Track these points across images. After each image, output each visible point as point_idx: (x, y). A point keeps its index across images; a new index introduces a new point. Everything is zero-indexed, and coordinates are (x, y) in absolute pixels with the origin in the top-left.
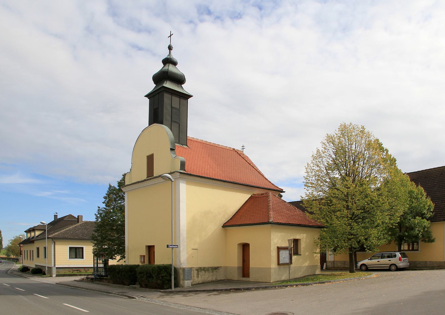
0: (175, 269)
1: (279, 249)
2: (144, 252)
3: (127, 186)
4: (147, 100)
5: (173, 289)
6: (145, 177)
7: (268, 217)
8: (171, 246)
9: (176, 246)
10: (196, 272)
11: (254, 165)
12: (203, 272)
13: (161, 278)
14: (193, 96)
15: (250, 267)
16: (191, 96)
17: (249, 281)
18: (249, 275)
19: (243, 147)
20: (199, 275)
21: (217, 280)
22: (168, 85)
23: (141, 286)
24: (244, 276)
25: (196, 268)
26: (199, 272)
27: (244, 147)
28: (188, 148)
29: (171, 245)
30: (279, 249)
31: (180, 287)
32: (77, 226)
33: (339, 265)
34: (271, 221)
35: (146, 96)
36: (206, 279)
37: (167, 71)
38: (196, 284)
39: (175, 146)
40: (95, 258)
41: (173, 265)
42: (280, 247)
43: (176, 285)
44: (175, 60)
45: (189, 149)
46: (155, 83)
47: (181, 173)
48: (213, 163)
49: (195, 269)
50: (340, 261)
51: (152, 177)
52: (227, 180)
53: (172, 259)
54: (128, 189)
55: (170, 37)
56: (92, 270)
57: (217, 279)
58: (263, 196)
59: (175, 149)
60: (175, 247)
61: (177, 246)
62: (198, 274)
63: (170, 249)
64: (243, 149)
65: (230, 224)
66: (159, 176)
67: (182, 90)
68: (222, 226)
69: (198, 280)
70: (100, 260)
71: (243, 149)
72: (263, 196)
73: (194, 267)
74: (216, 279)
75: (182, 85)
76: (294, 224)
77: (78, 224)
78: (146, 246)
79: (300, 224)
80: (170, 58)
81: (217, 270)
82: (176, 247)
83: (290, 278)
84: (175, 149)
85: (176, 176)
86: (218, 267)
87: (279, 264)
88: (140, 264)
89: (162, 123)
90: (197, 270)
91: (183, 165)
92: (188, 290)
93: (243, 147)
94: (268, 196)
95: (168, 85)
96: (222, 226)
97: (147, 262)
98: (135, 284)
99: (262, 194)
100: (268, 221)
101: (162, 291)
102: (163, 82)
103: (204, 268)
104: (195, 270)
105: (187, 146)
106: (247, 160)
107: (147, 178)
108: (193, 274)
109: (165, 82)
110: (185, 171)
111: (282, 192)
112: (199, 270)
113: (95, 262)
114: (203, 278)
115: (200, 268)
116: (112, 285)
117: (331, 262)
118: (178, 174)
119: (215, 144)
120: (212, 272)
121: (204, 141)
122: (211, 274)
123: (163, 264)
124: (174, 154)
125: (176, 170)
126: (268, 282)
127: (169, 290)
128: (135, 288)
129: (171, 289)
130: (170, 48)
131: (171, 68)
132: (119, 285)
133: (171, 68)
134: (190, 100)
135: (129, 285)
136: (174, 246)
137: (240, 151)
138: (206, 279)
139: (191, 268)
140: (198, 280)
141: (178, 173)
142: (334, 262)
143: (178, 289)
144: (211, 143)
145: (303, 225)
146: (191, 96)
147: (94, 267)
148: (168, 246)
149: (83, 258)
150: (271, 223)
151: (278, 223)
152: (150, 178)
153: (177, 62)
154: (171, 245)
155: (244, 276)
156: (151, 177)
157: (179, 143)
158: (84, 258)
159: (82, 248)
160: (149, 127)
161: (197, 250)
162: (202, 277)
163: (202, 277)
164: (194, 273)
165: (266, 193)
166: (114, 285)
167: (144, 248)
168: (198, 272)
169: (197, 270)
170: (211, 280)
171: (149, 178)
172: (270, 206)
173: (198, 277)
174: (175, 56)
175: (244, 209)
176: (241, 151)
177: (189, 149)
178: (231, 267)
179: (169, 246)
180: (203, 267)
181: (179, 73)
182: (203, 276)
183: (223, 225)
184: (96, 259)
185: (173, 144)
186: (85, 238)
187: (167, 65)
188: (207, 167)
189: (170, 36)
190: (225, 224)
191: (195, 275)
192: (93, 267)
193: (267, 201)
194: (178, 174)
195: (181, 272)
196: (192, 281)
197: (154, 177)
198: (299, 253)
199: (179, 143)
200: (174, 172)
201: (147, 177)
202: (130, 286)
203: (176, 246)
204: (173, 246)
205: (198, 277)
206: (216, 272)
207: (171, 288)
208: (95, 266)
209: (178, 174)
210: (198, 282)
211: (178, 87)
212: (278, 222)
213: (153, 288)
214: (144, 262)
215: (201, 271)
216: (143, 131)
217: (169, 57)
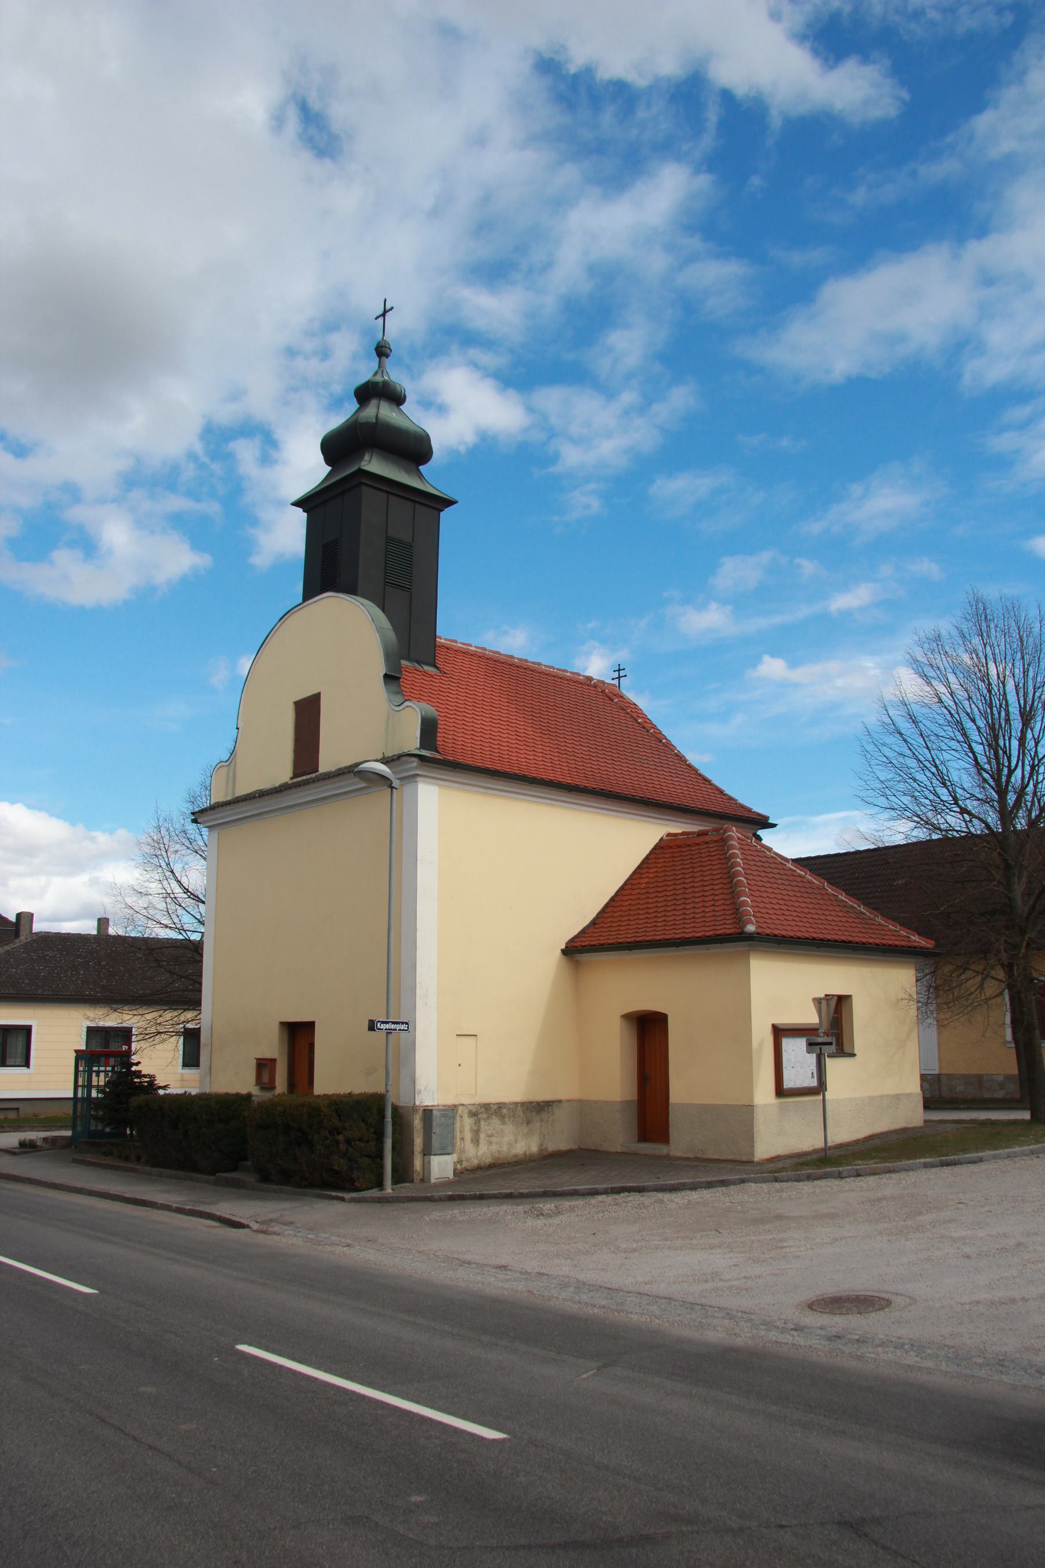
0: (395, 1109)
1: (779, 1033)
2: (272, 1047)
3: (218, 806)
4: (300, 516)
5: (389, 1189)
6: (282, 771)
7: (739, 918)
8: (383, 1026)
9: (403, 1023)
10: (468, 1122)
11: (658, 732)
12: (495, 1121)
13: (343, 1147)
14: (457, 502)
15: (671, 1100)
16: (449, 503)
17: (667, 1157)
18: (668, 1134)
19: (619, 670)
20: (482, 1136)
21: (546, 1153)
22: (374, 465)
23: (265, 1178)
24: (644, 1135)
25: (470, 1107)
26: (482, 1122)
27: (622, 673)
28: (440, 674)
29: (383, 1022)
30: (779, 1033)
31: (412, 1181)
32: (15, 948)
33: (959, 1089)
34: (751, 928)
35: (297, 504)
36: (505, 1148)
37: (374, 421)
38: (471, 1170)
39: (399, 668)
40: (81, 1069)
41: (391, 1099)
42: (781, 1027)
43: (402, 1174)
44: (398, 388)
45: (443, 678)
46: (328, 460)
47: (421, 758)
48: (525, 724)
49: (467, 1111)
50: (964, 1076)
51: (313, 775)
52: (584, 783)
53: (387, 1075)
54: (222, 818)
55: (381, 320)
56: (69, 1109)
57: (546, 1149)
58: (706, 839)
59: (399, 678)
60: (398, 1027)
61: (407, 1023)
62: (476, 1132)
63: (379, 1036)
64: (619, 678)
65: (592, 943)
66: (341, 772)
67: (421, 484)
68: (562, 950)
69: (479, 1154)
70: (98, 1076)
71: (619, 678)
72: (706, 839)
73: (463, 1105)
74: (541, 1150)
75: (421, 468)
76: (829, 940)
77: (17, 941)
78: (282, 1024)
79: (850, 942)
80: (386, 384)
81: (544, 1115)
82: (403, 1027)
83: (830, 1144)
84: (399, 678)
85: (407, 770)
86: (549, 1102)
87: (781, 1091)
88: (255, 1091)
89: (351, 590)
90: (473, 1114)
91: (429, 729)
92: (448, 1196)
93: (619, 670)
94: (723, 841)
95: (374, 465)
96: (562, 950)
97: (281, 1084)
98: (235, 1169)
99: (701, 834)
100: (739, 931)
101: (347, 1196)
102: (361, 458)
103: (500, 1106)
104: (465, 1116)
105: (436, 667)
106: (634, 715)
107: (292, 778)
108: (461, 1132)
109: (367, 457)
110: (437, 751)
111: (764, 823)
112: (479, 1116)
113: (80, 1083)
114: (494, 1148)
115: (486, 1107)
116: (148, 1168)
117: (929, 1077)
118: (415, 762)
119: (526, 661)
120: (528, 1122)
121: (490, 651)
122: (525, 1131)
123: (350, 1093)
124: (397, 693)
125: (406, 750)
126: (745, 1159)
127: (374, 1193)
128: (237, 1184)
129: (381, 1190)
130: (382, 351)
131: (386, 412)
132: (172, 1172)
133: (386, 412)
134: (446, 516)
135: (212, 1173)
136: (394, 1023)
137: (608, 684)
138: (505, 1148)
139: (454, 1108)
140: (479, 1154)
141: (413, 759)
142: (939, 1079)
143: (406, 1189)
144: (512, 657)
145: (857, 943)
146: (449, 503)
147: (75, 1098)
148: (372, 1026)
149: (27, 1064)
150: (750, 938)
151: (775, 935)
152: (304, 778)
153: (405, 395)
154: (383, 1022)
155: (644, 1135)
156: (309, 774)
157: (409, 657)
158: (31, 1067)
159: (28, 1030)
160: (305, 604)
161: (472, 1039)
162: (491, 1143)
163: (491, 1143)
164: (462, 1126)
165: (716, 830)
166: (155, 1170)
167: (276, 1028)
168: (478, 1122)
169: (473, 1114)
170: (525, 1153)
171: (300, 779)
172: (737, 874)
173: (476, 1141)
174: (396, 376)
175: (639, 886)
176: (614, 685)
177: (443, 678)
178: (595, 1102)
179: (379, 1025)
180: (494, 1104)
181: (412, 428)
182: (494, 1139)
183: (566, 947)
184: (84, 1071)
185: (393, 658)
186: (39, 992)
187: (374, 402)
188: (509, 740)
189: (384, 315)
190: (572, 940)
191: (468, 1136)
192: (71, 1095)
193: (721, 857)
194: (412, 762)
195: (417, 1122)
196: (454, 1157)
197: (318, 773)
198: (846, 1049)
199: (408, 659)
200: (400, 756)
201: (295, 775)
202: (218, 1174)
203: (403, 1023)
204: (393, 1026)
205: (476, 1141)
206: (542, 1120)
207: (380, 1184)
208: (80, 1095)
209: (415, 764)
210: (475, 1162)
211: (408, 472)
212: (776, 932)
213: (312, 1185)
214: (270, 1086)
215: (488, 1118)
216: (284, 619)
217: (379, 379)
